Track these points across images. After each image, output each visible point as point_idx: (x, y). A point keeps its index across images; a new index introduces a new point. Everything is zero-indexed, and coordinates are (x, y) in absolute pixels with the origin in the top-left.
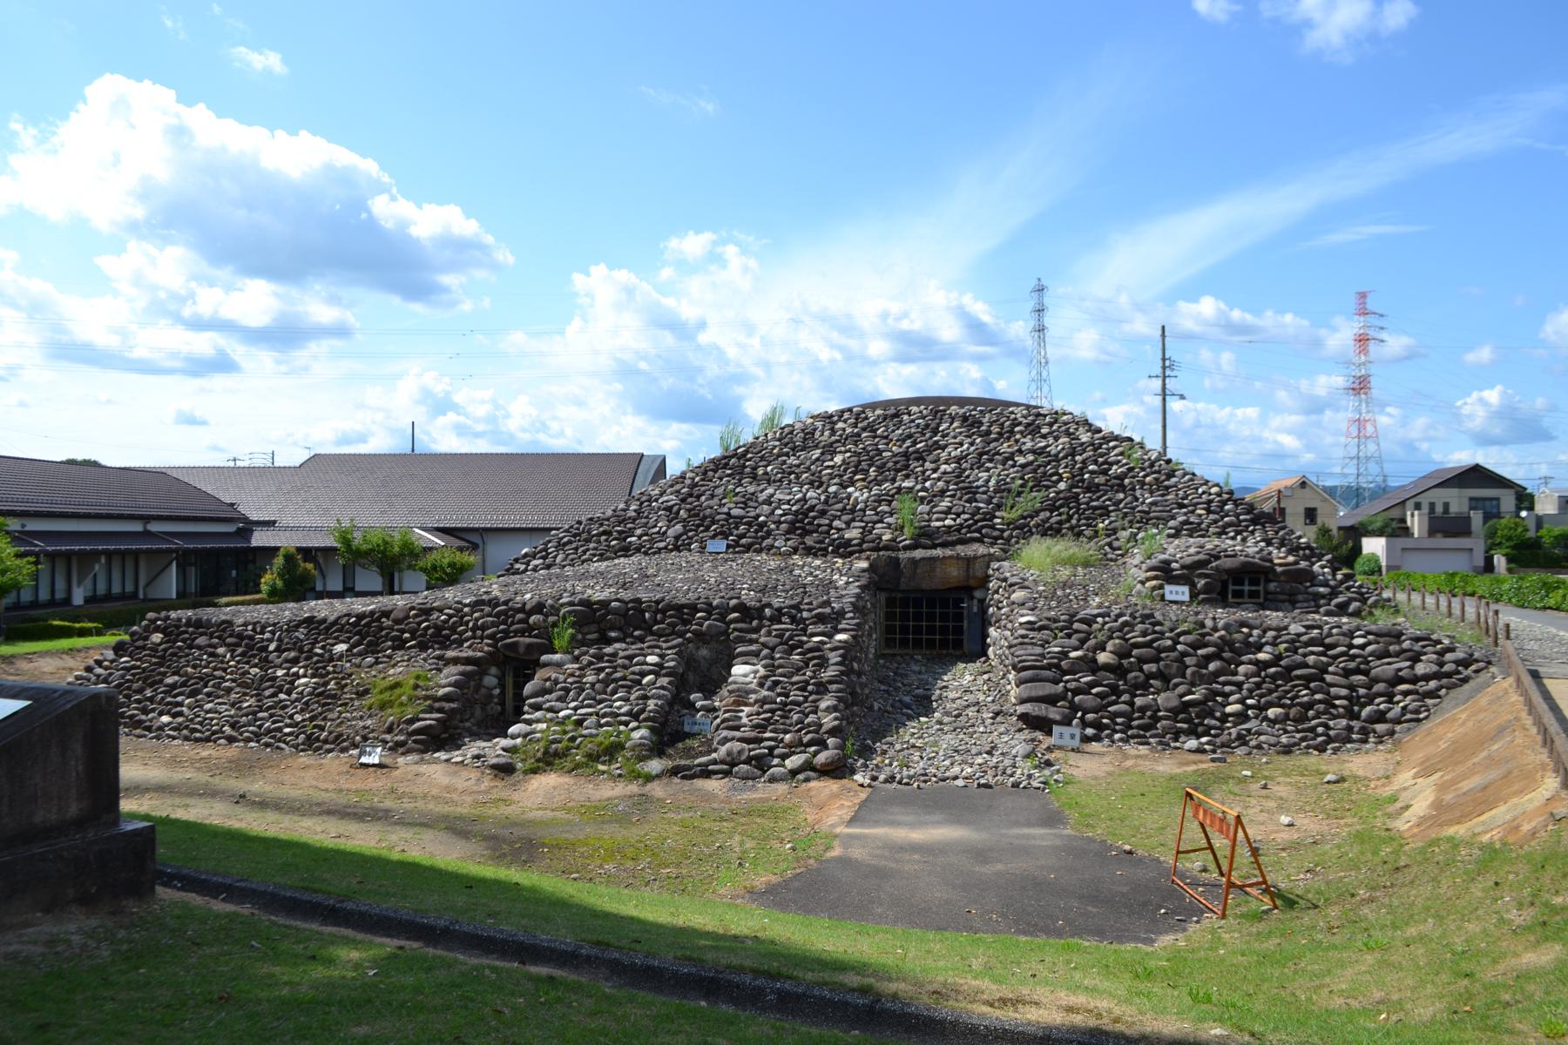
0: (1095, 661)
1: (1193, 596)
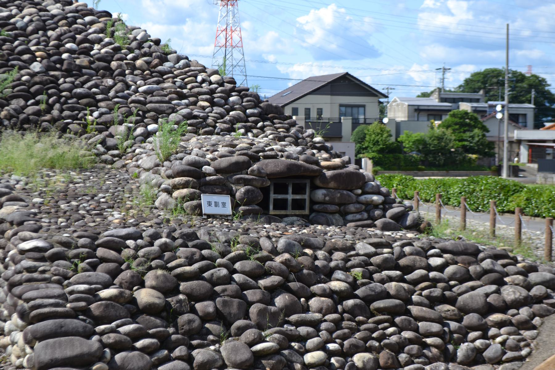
0: (133, 301)
1: (235, 206)
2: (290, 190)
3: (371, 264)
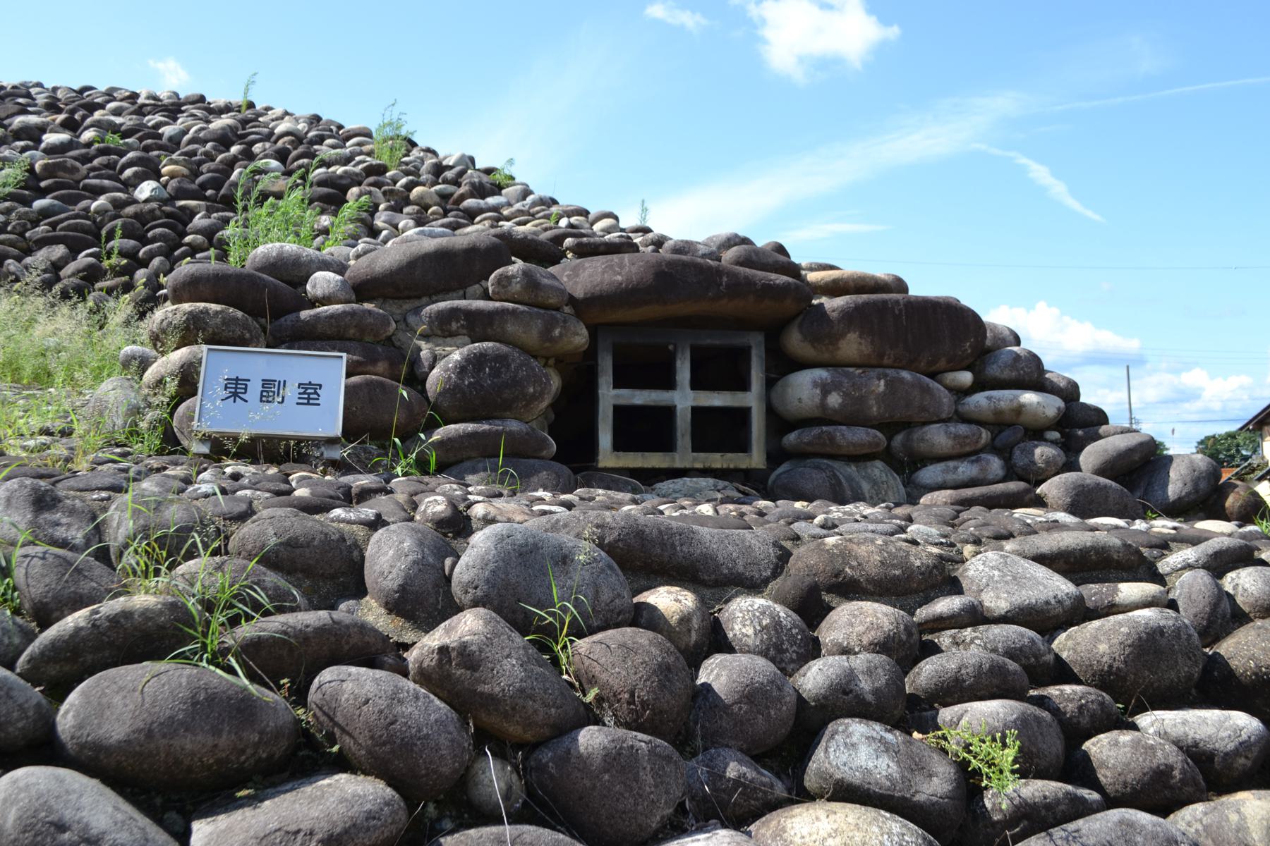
2: (684, 372)
3: (1062, 672)
